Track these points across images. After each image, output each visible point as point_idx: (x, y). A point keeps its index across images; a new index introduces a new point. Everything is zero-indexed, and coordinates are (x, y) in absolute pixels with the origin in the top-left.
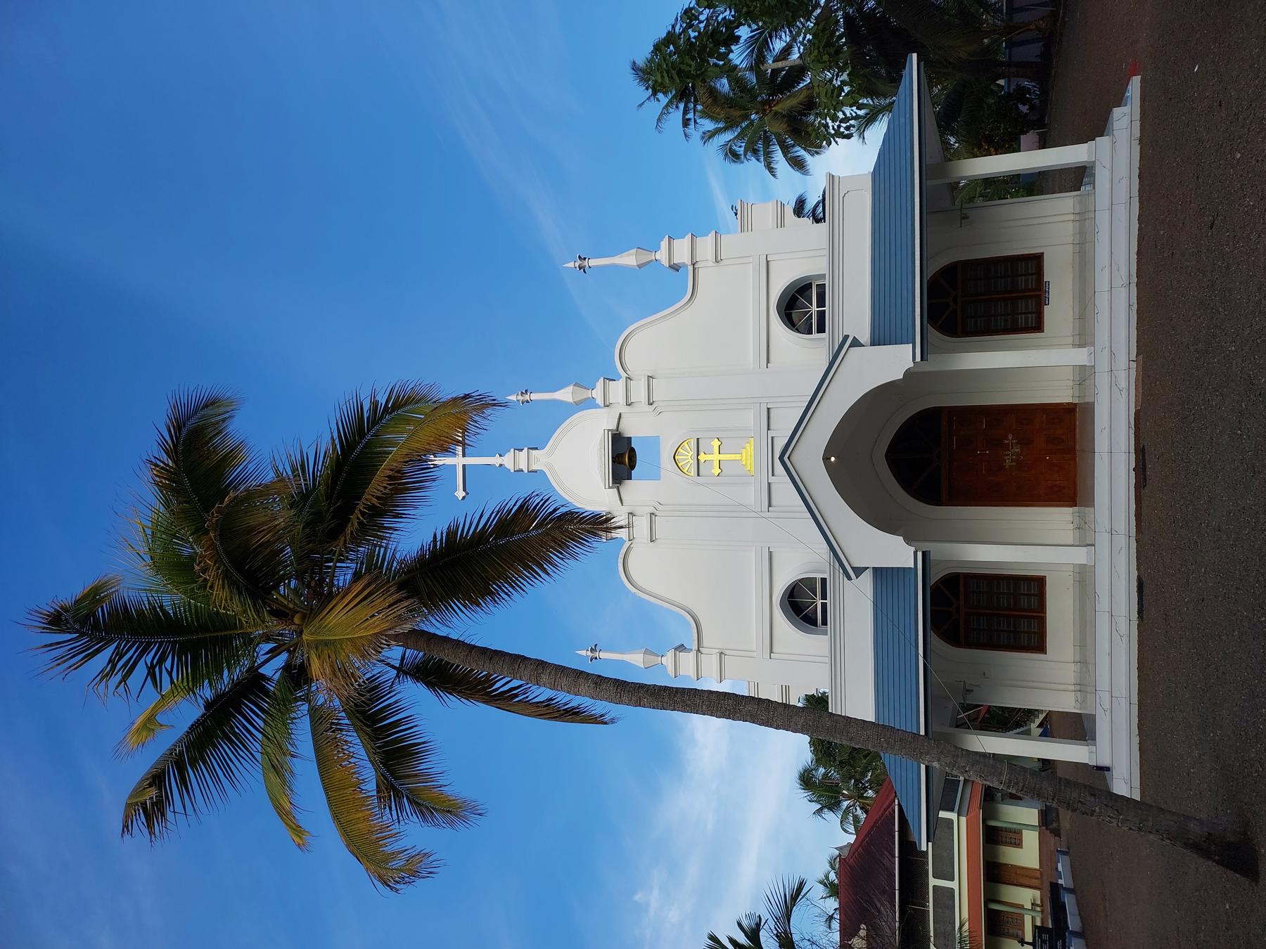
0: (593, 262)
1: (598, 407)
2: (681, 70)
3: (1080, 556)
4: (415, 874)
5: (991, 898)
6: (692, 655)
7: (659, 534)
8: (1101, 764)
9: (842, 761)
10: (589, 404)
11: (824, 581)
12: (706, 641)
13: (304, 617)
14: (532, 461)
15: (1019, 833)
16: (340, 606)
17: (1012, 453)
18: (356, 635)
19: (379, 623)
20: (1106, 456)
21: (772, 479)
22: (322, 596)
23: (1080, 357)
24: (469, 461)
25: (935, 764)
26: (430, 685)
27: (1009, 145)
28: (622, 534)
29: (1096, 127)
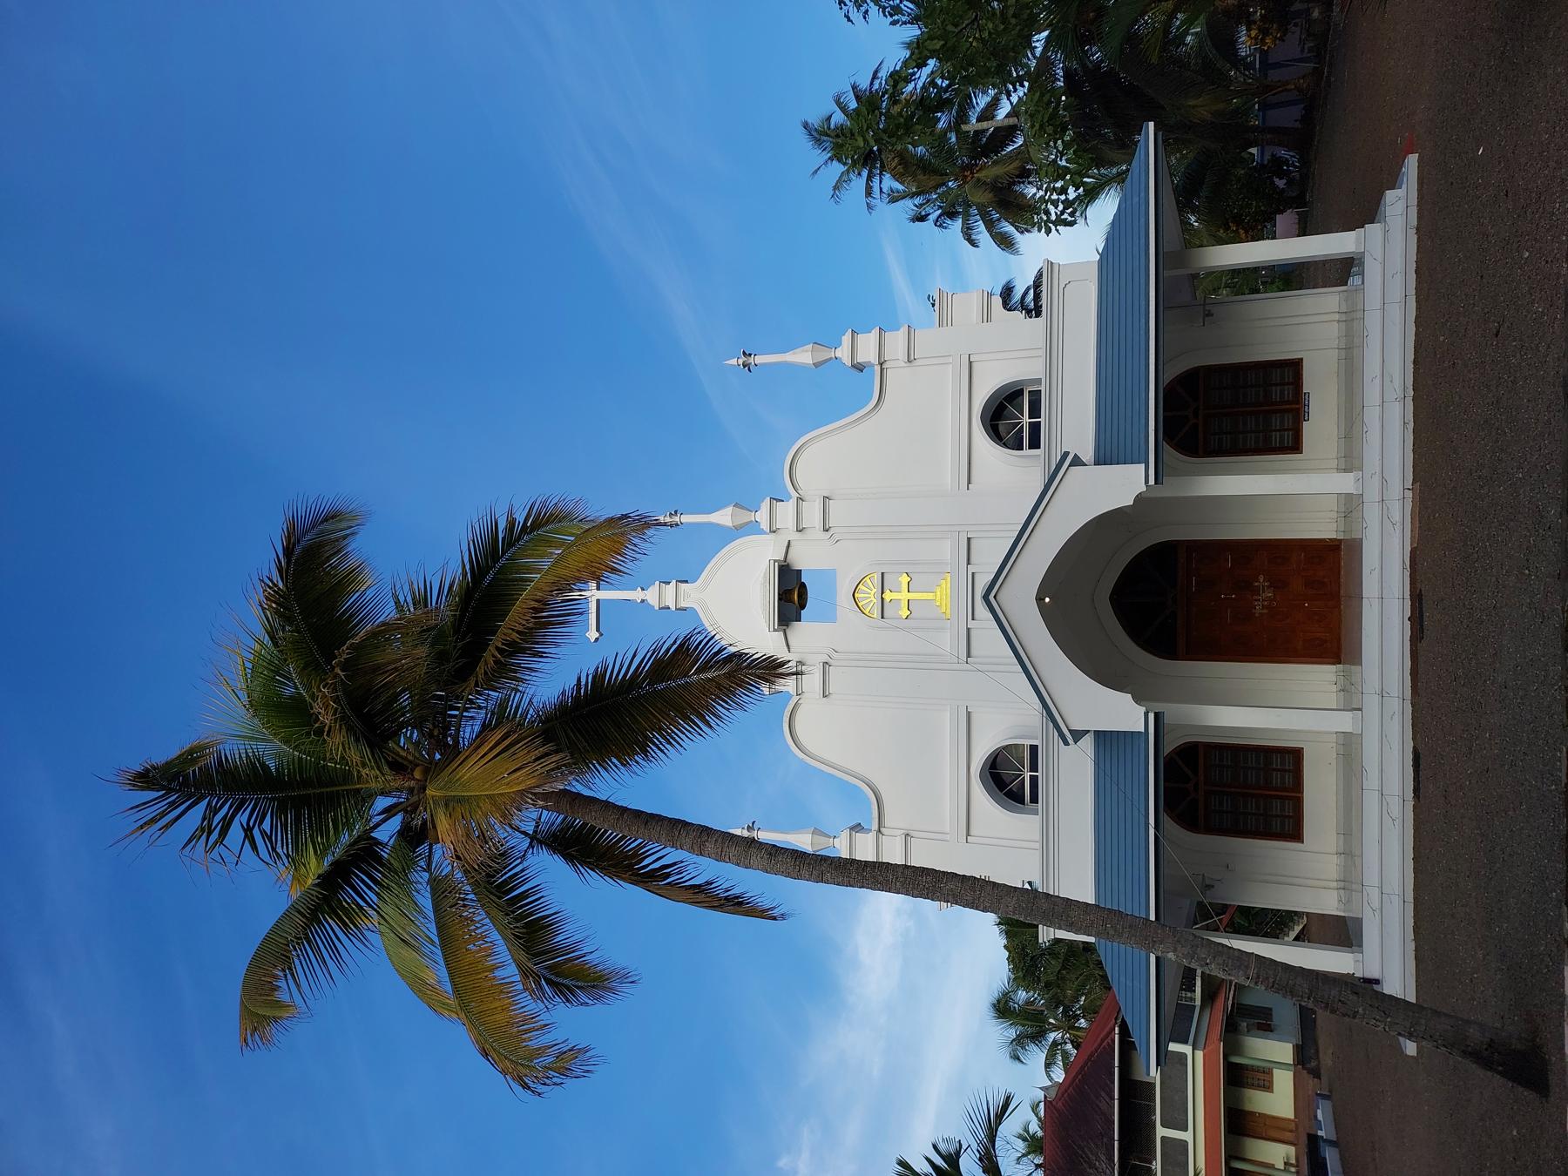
0: (759, 359)
1: (762, 532)
2: (882, 138)
3: (1344, 722)
4: (565, 1072)
5: (1233, 1154)
6: (871, 836)
7: (832, 689)
8: (1368, 975)
9: (1051, 974)
10: (751, 528)
11: (1034, 749)
12: (888, 821)
13: (426, 771)
14: (681, 599)
15: (1269, 1073)
16: (475, 758)
17: (1265, 596)
18: (494, 796)
19: (523, 780)
20: (1376, 603)
21: (971, 624)
22: (450, 744)
23: (1345, 483)
24: (604, 595)
25: (1171, 955)
26: (569, 858)
27: (1258, 230)
28: (788, 685)
29: (1364, 213)
